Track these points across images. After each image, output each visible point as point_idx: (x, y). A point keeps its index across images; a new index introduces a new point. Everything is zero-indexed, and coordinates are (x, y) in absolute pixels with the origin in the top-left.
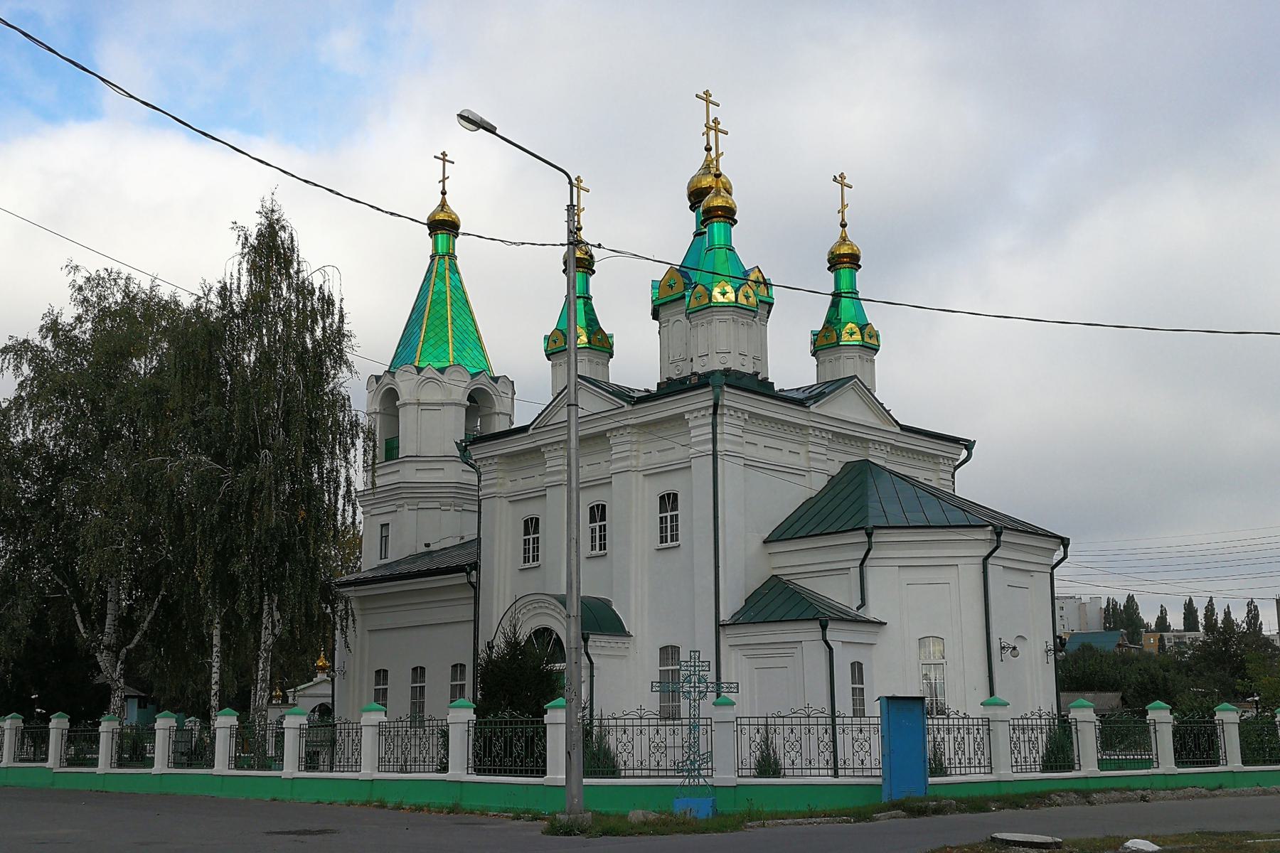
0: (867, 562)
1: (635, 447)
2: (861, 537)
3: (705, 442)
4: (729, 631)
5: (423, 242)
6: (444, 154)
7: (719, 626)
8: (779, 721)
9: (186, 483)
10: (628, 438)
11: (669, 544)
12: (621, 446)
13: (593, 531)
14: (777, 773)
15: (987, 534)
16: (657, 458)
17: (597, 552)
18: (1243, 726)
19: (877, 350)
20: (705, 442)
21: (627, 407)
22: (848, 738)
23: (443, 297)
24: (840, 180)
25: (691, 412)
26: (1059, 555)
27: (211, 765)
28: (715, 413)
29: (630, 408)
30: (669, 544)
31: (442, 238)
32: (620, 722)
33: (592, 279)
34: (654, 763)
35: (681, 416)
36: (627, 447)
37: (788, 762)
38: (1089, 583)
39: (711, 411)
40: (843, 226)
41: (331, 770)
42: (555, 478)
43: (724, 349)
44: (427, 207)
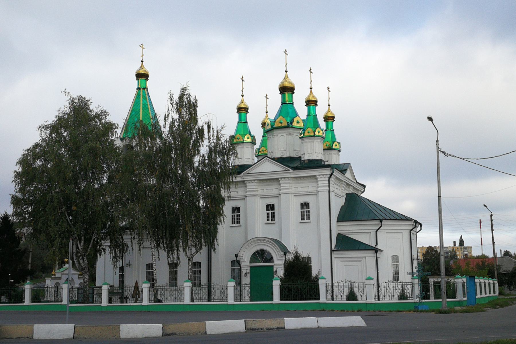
0: (379, 231)
1: (291, 185)
2: (378, 222)
3: (326, 186)
4: (335, 252)
5: (134, 83)
6: (142, 45)
7: (332, 251)
8: (337, 284)
9: (126, 188)
10: (289, 182)
11: (305, 221)
12: (284, 185)
13: (268, 214)
14: (406, 299)
15: (412, 223)
16: (300, 190)
17: (270, 222)
18: (32, 290)
19: (324, 149)
20: (326, 186)
21: (291, 171)
22: (337, 289)
23: (147, 106)
24: (430, 119)
25: (319, 175)
26: (419, 228)
27: (272, 299)
28: (330, 177)
29: (292, 171)
30: (305, 221)
31: (143, 81)
32: (387, 284)
33: (248, 115)
34: (340, 296)
35: (315, 176)
36: (289, 185)
37: (360, 296)
38: (427, 238)
39: (328, 176)
40: (142, 62)
41: (241, 301)
42: (251, 193)
43: (309, 152)
44: (135, 68)
